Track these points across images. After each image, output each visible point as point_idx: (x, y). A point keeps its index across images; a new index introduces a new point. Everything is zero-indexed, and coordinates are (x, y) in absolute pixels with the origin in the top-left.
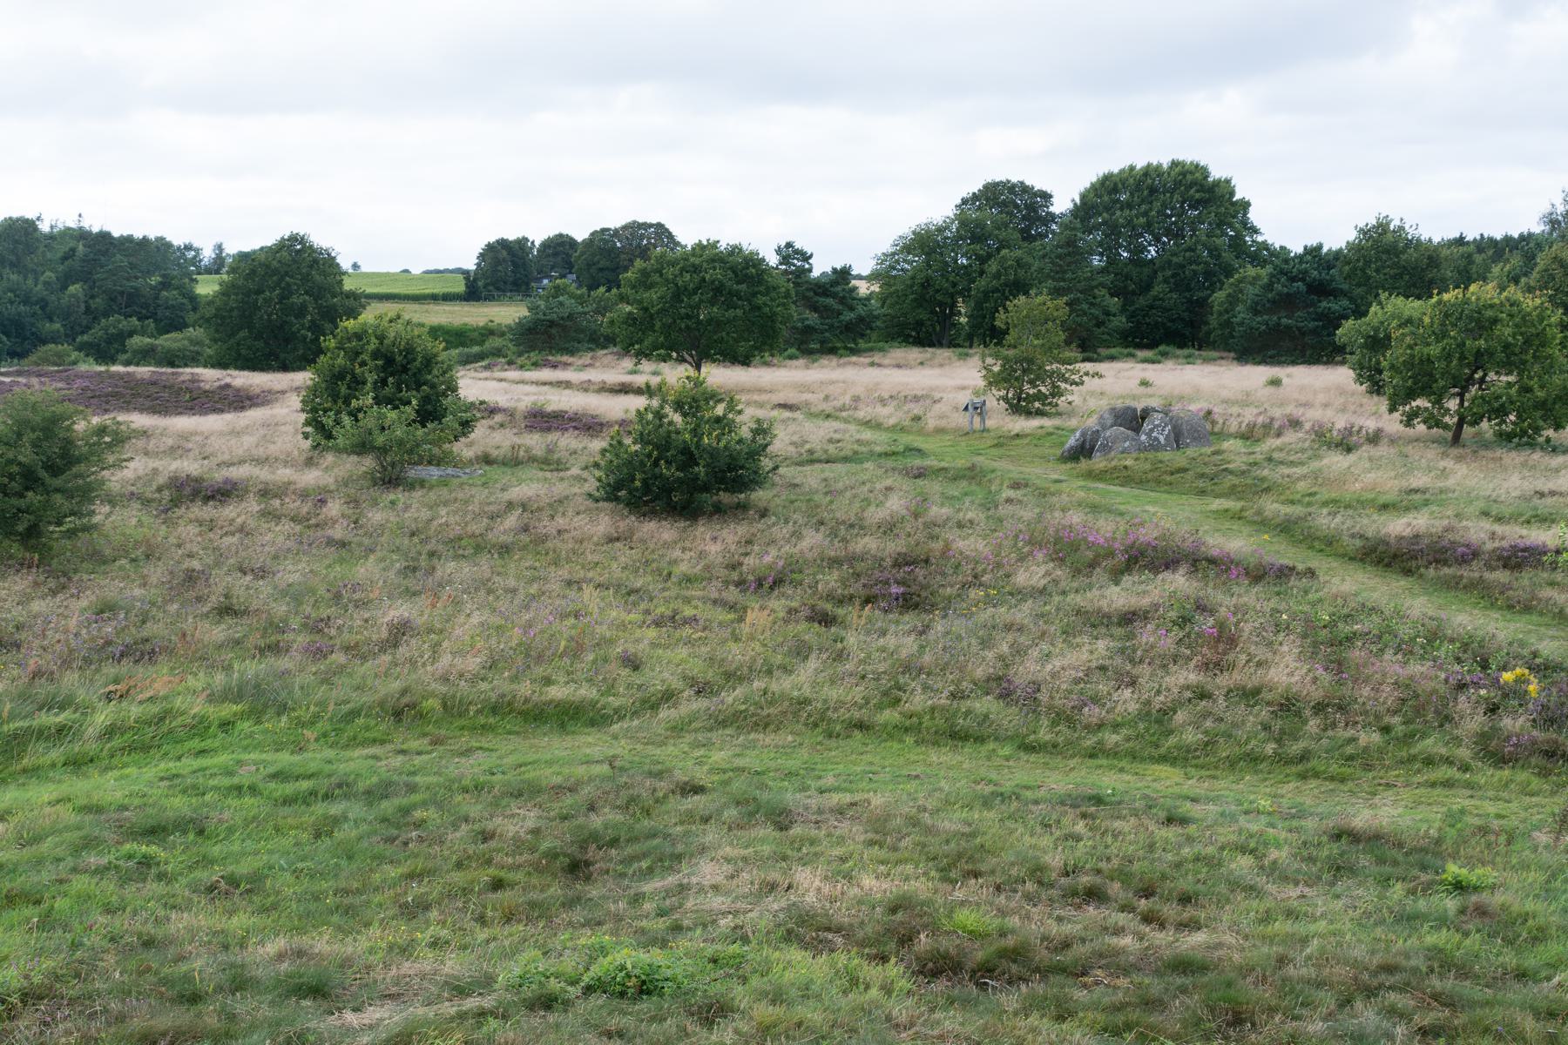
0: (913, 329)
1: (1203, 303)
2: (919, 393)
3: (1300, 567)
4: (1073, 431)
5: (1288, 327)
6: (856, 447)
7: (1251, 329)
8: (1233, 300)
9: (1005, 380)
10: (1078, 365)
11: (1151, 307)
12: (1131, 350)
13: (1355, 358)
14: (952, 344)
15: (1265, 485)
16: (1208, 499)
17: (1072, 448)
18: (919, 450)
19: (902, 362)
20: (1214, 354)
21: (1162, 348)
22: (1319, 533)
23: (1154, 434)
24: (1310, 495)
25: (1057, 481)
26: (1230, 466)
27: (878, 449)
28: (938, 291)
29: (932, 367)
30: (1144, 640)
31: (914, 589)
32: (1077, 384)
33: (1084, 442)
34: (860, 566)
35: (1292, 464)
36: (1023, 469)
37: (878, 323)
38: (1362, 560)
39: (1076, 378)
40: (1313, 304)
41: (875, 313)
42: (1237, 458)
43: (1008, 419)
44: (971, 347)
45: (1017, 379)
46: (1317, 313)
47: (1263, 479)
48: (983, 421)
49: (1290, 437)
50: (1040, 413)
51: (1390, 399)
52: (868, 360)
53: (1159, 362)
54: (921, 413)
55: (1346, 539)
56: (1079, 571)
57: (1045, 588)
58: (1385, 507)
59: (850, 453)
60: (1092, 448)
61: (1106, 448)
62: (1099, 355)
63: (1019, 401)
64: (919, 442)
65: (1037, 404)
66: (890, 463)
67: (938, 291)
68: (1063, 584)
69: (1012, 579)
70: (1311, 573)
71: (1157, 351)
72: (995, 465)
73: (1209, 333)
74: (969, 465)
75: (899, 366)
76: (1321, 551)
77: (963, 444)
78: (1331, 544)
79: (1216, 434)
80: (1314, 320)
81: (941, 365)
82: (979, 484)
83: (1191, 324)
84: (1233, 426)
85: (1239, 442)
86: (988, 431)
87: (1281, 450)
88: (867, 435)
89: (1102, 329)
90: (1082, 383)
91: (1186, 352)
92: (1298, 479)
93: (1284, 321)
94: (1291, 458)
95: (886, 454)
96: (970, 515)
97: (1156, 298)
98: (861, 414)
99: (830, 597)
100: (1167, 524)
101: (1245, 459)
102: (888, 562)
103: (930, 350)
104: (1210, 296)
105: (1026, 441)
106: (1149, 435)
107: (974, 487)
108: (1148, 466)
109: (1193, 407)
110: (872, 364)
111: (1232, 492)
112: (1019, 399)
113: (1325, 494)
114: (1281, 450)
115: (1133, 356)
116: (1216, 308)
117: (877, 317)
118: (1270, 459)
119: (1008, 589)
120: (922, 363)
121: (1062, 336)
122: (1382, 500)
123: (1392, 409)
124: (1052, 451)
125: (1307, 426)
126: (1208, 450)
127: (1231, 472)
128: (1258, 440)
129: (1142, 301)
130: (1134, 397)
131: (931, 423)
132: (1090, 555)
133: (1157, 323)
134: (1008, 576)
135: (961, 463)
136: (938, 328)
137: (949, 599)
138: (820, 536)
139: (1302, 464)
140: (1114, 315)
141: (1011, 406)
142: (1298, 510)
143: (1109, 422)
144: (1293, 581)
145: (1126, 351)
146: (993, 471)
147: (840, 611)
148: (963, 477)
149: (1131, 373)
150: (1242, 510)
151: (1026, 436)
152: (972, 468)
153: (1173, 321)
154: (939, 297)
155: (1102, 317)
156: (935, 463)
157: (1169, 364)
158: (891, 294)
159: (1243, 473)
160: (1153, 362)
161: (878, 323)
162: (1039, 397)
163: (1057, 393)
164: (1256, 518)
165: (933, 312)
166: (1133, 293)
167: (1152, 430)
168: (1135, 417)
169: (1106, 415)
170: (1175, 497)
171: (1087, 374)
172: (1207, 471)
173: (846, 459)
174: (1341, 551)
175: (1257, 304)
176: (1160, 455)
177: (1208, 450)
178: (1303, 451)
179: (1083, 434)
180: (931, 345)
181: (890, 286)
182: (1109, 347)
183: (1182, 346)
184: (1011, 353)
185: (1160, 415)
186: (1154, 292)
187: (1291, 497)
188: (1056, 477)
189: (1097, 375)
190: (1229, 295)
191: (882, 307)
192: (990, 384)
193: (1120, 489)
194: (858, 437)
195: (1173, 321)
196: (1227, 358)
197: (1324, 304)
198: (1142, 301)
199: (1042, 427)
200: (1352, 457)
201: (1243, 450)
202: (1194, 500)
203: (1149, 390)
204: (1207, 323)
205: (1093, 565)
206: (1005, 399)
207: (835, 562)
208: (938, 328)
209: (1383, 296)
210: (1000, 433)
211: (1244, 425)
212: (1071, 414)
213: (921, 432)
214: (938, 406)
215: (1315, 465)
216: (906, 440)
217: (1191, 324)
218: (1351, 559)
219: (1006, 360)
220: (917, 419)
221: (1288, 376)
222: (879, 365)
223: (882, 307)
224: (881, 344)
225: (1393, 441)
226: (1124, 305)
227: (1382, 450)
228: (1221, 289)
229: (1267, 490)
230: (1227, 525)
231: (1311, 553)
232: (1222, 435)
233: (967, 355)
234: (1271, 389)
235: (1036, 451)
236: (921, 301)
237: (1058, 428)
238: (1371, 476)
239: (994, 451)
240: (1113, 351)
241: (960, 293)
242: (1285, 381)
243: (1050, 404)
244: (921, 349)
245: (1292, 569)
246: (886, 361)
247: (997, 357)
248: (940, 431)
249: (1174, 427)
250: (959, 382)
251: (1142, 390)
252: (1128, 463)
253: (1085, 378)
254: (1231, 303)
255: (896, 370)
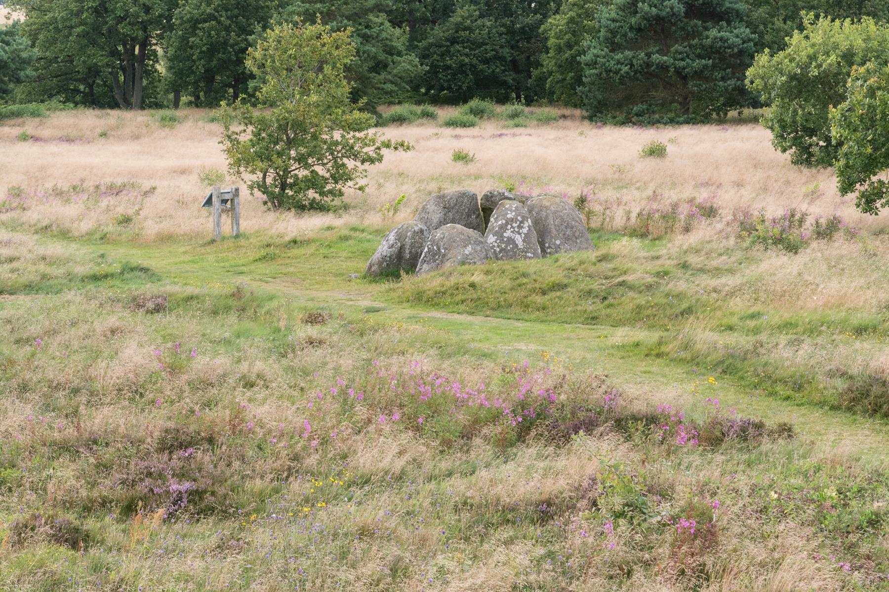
0: (83, 80)
1: (530, 34)
2: (119, 181)
3: (771, 423)
4: (380, 233)
5: (664, 68)
6: (42, 267)
7: (608, 71)
8: (576, 29)
9: (260, 156)
10: (371, 131)
11: (453, 41)
12: (431, 108)
13: (769, 112)
14: (149, 102)
15: (684, 306)
16: (605, 330)
17: (384, 258)
18: (145, 270)
19: (74, 133)
20: (553, 111)
21: (474, 103)
22: (780, 373)
23: (508, 234)
24: (753, 316)
25: (370, 310)
26: (629, 278)
27: (81, 270)
28: (121, 19)
29: (121, 139)
30: (578, 541)
31: (202, 484)
32: (372, 161)
33: (402, 249)
34: (108, 454)
35: (717, 272)
36: (313, 294)
37: (29, 71)
38: (849, 409)
39: (370, 150)
40: (695, 34)
41: (24, 55)
42: (635, 266)
43: (271, 216)
44: (176, 105)
45: (280, 154)
46: (703, 47)
47: (680, 296)
48: (236, 220)
49: (703, 231)
50: (316, 207)
51: (841, 173)
52: (16, 131)
53: (472, 125)
54: (130, 212)
55: (822, 381)
56: (447, 444)
57: (403, 472)
58: (860, 331)
59: (35, 278)
60: (415, 257)
61: (437, 257)
62: (380, 116)
63: (283, 188)
64: (138, 258)
65: (311, 194)
66: (105, 291)
67: (121, 19)
68: (428, 466)
69: (352, 462)
70: (786, 430)
71: (466, 107)
72: (270, 288)
73: (542, 79)
74: (228, 290)
75: (69, 140)
76: (788, 398)
77: (211, 258)
78: (799, 388)
79: (593, 231)
80: (700, 56)
81: (136, 137)
82: (255, 318)
83: (514, 65)
84: (619, 221)
85: (636, 242)
86: (246, 237)
87: (697, 251)
88: (56, 248)
89: (383, 76)
90: (380, 159)
91: (509, 108)
92: (732, 294)
93: (656, 58)
94: (715, 263)
95: (95, 278)
96: (259, 366)
97: (459, 27)
98: (33, 215)
99: (68, 505)
100: (161, 423)
101: (650, 266)
102: (151, 443)
103: (114, 113)
104: (541, 22)
105: (311, 249)
106: (499, 234)
107: (247, 324)
108: (507, 283)
109: (556, 188)
110: (24, 138)
111: (638, 317)
112: (284, 186)
113: (774, 315)
114: (697, 251)
115: (427, 115)
116: (552, 42)
117: (27, 62)
118: (685, 266)
119: (348, 476)
120: (104, 135)
121: (345, 89)
122: (856, 320)
123: (846, 187)
124: (351, 264)
125: (726, 215)
126: (592, 255)
127: (631, 288)
128: (659, 238)
129: (438, 32)
130: (452, 180)
131: (152, 228)
132: (462, 418)
133: (462, 65)
134: (344, 457)
135: (218, 287)
136: (122, 78)
137: (261, 497)
138: (28, 409)
139: (731, 271)
140: (399, 54)
141: (272, 196)
142: (739, 341)
143: (436, 217)
144: (766, 445)
145: (419, 109)
146: (271, 298)
147: (90, 524)
148: (227, 309)
149: (433, 143)
150: (660, 343)
151: (308, 242)
152: (237, 294)
153: (486, 61)
154: (123, 28)
155: (382, 56)
156: (176, 289)
157: (488, 128)
158: (45, 25)
159: (649, 287)
160: (464, 125)
161: (29, 71)
162: (314, 182)
163: (341, 175)
164: (683, 355)
165: (114, 53)
166: (425, 21)
167: (503, 228)
168: (473, 209)
169: (431, 207)
170: (555, 327)
171: (387, 145)
172: (595, 286)
173: (29, 288)
174: (817, 397)
175: (614, 33)
176: (522, 265)
177: (592, 255)
178: (727, 252)
179: (400, 237)
180: (114, 105)
181: (45, 12)
182: (391, 103)
183: (502, 100)
184: (268, 114)
185: (515, 204)
186: (455, 19)
187: (725, 321)
188: (366, 303)
189: (401, 146)
190: (571, 20)
191: (33, 46)
192: (238, 163)
193: (470, 318)
194: (41, 251)
195: (486, 61)
196: (572, 117)
197: (713, 33)
198: (438, 32)
199: (329, 228)
200: (801, 259)
201: (643, 254)
202: (582, 330)
203: (472, 168)
204: (538, 64)
205: (467, 434)
206: (262, 187)
207: (64, 448)
208: (122, 78)
209: (807, 17)
210: (267, 239)
211: (634, 215)
212: (366, 207)
213: (136, 241)
214: (152, 200)
215: (750, 272)
216: (118, 256)
217: (514, 65)
218: (833, 408)
219: (263, 124)
220: (126, 220)
221: (671, 141)
222: (36, 139)
223: (33, 46)
224: (33, 106)
225: (852, 234)
226: (412, 39)
227: (840, 246)
228: (557, 12)
229: (689, 311)
230: (642, 366)
231: (773, 403)
232: (602, 233)
233: (173, 119)
234: (652, 163)
235: (328, 265)
236: (91, 37)
237: (354, 229)
238: (834, 286)
239: (263, 268)
240: (397, 110)
241: (157, 22)
242: (670, 149)
243: (331, 192)
244: (98, 112)
245: (759, 426)
246: (45, 133)
247: (248, 121)
248: (166, 239)
249: (536, 223)
250: (173, 162)
251: (460, 168)
252: (477, 278)
253: (384, 151)
254: (574, 33)
255: (64, 147)
